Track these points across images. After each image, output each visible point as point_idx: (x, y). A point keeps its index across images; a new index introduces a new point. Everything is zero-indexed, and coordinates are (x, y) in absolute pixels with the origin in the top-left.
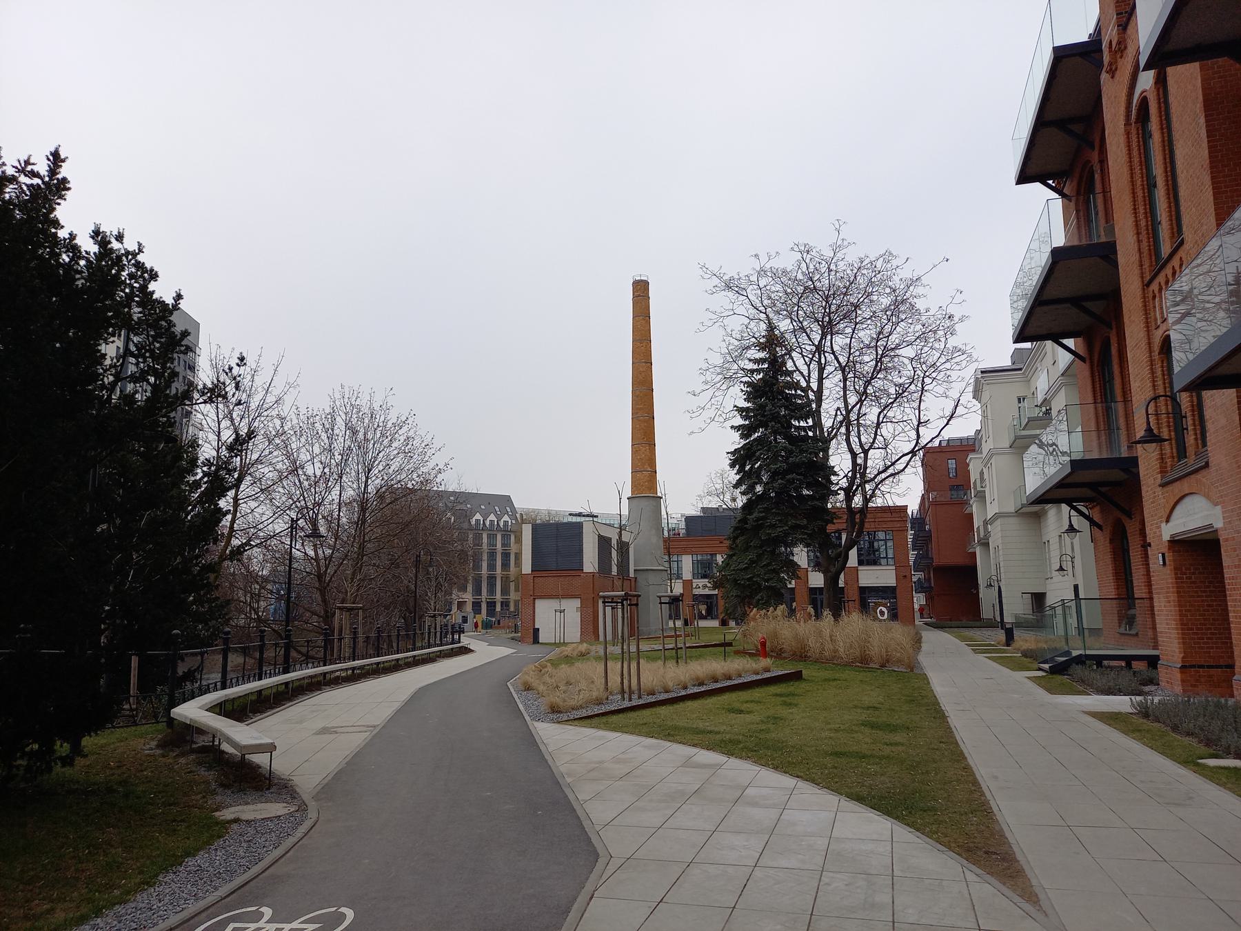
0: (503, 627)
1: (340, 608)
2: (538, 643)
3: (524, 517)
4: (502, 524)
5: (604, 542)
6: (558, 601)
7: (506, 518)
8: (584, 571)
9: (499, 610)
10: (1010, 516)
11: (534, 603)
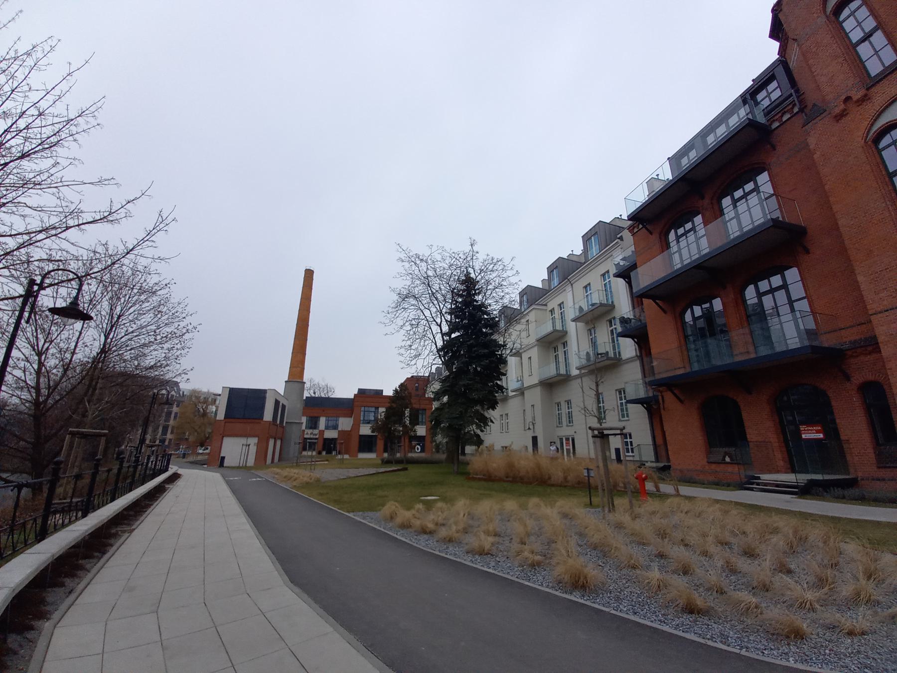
1: (73, 434)
2: (223, 466)
5: (277, 402)
6: (245, 439)
7: (173, 393)
11: (222, 439)
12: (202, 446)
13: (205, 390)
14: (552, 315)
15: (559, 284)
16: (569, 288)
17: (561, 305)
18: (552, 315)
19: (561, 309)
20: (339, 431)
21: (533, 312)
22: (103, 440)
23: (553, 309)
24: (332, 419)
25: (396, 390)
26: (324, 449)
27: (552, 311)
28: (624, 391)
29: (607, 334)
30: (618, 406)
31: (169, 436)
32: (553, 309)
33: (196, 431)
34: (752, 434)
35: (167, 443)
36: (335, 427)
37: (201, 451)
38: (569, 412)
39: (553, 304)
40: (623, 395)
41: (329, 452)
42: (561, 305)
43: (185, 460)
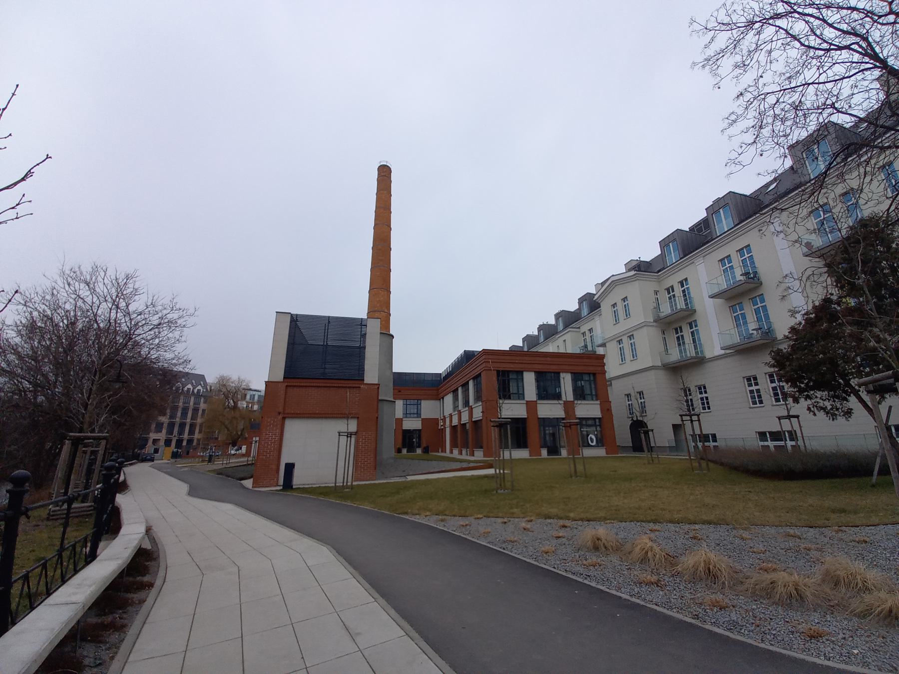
0: (193, 457)
3: (212, 388)
4: (196, 391)
7: (199, 387)
8: (365, 382)
9: (185, 444)
10: (721, 358)
12: (234, 446)
13: (235, 377)
14: (584, 337)
15: (588, 314)
16: (597, 318)
17: (591, 330)
18: (591, 333)
19: (591, 333)
20: (423, 419)
21: (570, 333)
22: (103, 442)
23: (585, 332)
25: (528, 339)
26: (404, 446)
27: (584, 334)
29: (731, 319)
30: (639, 404)
31: (197, 436)
32: (585, 332)
33: (226, 427)
34: (163, 432)
35: (195, 444)
36: (418, 414)
37: (233, 452)
38: (629, 404)
39: (585, 328)
40: (642, 396)
41: (411, 449)
42: (591, 330)
43: (211, 467)
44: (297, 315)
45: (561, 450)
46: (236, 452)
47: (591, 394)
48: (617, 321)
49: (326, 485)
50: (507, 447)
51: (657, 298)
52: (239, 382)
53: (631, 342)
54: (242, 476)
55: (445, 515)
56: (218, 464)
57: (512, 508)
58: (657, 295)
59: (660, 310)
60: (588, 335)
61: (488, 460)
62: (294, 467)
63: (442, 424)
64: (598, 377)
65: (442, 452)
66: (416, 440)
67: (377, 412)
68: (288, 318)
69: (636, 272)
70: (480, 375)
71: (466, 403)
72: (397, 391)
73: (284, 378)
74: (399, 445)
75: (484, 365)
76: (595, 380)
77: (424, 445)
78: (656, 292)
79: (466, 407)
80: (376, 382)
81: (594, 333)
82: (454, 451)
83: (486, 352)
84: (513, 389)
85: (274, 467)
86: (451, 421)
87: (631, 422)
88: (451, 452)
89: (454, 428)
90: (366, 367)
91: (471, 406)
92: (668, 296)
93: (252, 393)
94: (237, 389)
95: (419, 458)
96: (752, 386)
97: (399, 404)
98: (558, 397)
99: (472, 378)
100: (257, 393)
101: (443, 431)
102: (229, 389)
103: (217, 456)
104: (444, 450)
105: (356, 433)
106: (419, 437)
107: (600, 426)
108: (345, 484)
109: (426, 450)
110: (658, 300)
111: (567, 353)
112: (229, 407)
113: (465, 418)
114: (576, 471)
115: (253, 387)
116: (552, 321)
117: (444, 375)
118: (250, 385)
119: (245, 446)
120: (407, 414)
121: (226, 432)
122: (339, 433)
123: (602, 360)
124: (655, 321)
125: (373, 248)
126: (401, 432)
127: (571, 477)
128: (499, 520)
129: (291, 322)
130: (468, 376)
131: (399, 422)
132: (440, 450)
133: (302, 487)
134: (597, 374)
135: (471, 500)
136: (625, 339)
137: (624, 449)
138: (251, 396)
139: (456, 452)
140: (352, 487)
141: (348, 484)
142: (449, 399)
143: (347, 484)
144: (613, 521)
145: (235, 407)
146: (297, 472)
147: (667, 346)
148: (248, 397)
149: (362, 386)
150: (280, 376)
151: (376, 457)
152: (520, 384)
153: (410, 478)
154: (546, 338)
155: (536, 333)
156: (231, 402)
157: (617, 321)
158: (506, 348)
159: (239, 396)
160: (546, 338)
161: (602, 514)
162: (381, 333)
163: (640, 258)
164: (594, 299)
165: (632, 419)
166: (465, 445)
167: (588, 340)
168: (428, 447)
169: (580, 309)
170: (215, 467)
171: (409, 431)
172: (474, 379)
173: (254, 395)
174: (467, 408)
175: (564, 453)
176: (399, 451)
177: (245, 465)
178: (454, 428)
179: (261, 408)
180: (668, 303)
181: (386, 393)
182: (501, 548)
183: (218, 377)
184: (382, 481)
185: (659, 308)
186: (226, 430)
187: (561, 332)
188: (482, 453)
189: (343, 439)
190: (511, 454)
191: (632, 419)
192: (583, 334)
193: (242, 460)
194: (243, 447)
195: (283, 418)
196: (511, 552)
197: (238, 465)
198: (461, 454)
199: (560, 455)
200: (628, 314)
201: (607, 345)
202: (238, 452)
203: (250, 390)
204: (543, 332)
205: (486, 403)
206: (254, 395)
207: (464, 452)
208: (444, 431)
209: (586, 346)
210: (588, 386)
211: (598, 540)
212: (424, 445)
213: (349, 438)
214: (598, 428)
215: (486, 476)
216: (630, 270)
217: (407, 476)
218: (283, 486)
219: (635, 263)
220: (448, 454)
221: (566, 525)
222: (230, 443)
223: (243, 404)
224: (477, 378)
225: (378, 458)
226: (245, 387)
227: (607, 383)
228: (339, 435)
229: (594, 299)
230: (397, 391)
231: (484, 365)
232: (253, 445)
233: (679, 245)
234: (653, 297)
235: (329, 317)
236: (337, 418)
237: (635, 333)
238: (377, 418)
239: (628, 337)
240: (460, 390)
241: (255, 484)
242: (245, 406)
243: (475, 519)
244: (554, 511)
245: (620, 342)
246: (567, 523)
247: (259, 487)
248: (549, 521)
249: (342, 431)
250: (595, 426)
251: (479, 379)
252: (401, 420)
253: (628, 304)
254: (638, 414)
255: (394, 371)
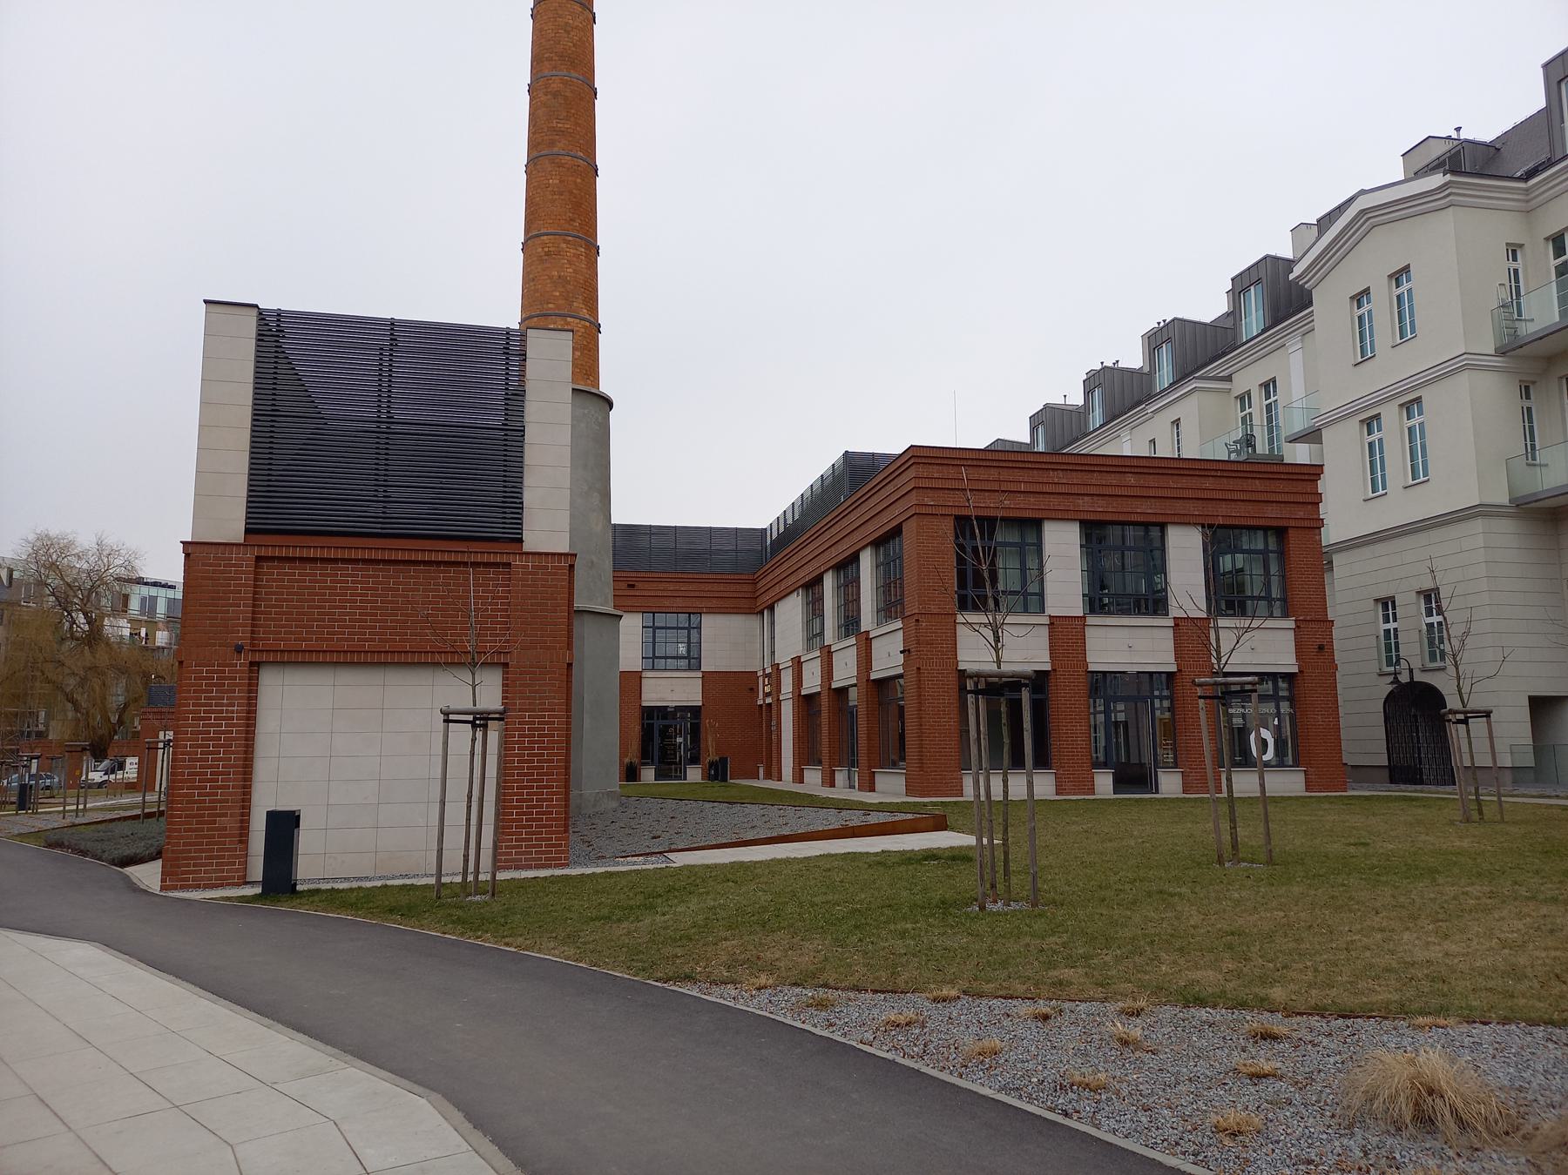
3: (16, 575)
8: (527, 547)
13: (85, 540)
15: (1264, 331)
17: (1269, 386)
18: (1268, 397)
19: (1268, 397)
20: (707, 677)
21: (1194, 397)
23: (1249, 393)
24: (671, 620)
25: (1046, 418)
27: (1244, 399)
28: (1394, 603)
32: (1249, 393)
37: (96, 777)
38: (1387, 632)
39: (1248, 379)
41: (669, 766)
42: (1269, 386)
43: (26, 822)
44: (279, 314)
45: (1160, 774)
46: (106, 778)
47: (1268, 598)
48: (1366, 355)
49: (408, 882)
50: (1018, 762)
51: (1516, 271)
52: (100, 558)
53: (1371, 439)
54: (128, 851)
55: (826, 986)
56: (50, 816)
57: (1052, 965)
58: (1515, 259)
59: (1520, 314)
60: (1258, 402)
61: (925, 805)
62: (298, 825)
63: (767, 689)
64: (1294, 538)
65: (768, 776)
66: (685, 740)
67: (569, 646)
68: (250, 323)
69: (1448, 177)
70: (897, 532)
71: (850, 624)
72: (624, 585)
73: (247, 531)
74: (633, 756)
75: (913, 499)
76: (1282, 554)
77: (710, 754)
78: (1513, 251)
79: (847, 636)
80: (563, 547)
81: (1280, 397)
82: (878, 778)
83: (918, 456)
84: (1008, 577)
85: (230, 822)
86: (798, 681)
87: (1390, 688)
88: (799, 777)
89: (807, 703)
90: (529, 497)
91: (867, 632)
92: (1554, 263)
93: (146, 591)
94: (95, 578)
95: (693, 794)
96: (1432, 616)
97: (632, 627)
98: (1155, 603)
99: (871, 544)
100: (162, 592)
101: (771, 712)
102: (69, 580)
103: (48, 788)
104: (775, 773)
105: (501, 716)
106: (695, 731)
107: (1291, 700)
108: (470, 878)
109: (717, 772)
110: (1517, 281)
111: (1179, 459)
112: (73, 637)
113: (845, 671)
114: (1235, 845)
115: (149, 574)
116: (1133, 358)
117: (775, 535)
118: (137, 563)
119: (136, 760)
120: (654, 657)
121: (70, 715)
122: (446, 714)
123: (1308, 487)
124: (1501, 352)
125: (532, 90)
126: (637, 714)
127: (1220, 861)
128: (1024, 1008)
129: (260, 337)
130: (856, 536)
131: (631, 682)
132: (761, 771)
133: (329, 886)
134: (1290, 531)
135: (903, 935)
136: (1391, 415)
137: (1361, 773)
138: (143, 600)
139: (813, 777)
140: (494, 888)
141: (482, 877)
142: (791, 611)
143: (476, 877)
144: (1441, 1021)
145: (94, 636)
146: (307, 841)
147: (1532, 439)
148: (134, 604)
149: (517, 562)
150: (231, 525)
151: (567, 794)
152: (1032, 563)
153: (680, 859)
154: (1111, 416)
155: (1077, 399)
156: (81, 619)
157: (1366, 355)
158: (981, 444)
159: (104, 602)
160: (1111, 416)
161: (1385, 994)
162: (573, 389)
163: (1458, 129)
164: (1291, 277)
165: (1396, 681)
166: (846, 755)
167: (1259, 418)
168: (723, 761)
169: (1234, 314)
170: (38, 823)
171: (662, 711)
172: (877, 544)
173: (154, 599)
174: (853, 641)
175: (1170, 783)
176: (631, 774)
177: (136, 817)
178: (807, 703)
179: (181, 638)
180: (1554, 284)
181: (594, 591)
182: (1051, 1109)
183: (32, 537)
184: (588, 871)
185: (1519, 305)
186: (69, 705)
187: (1164, 392)
188: (902, 781)
189: (462, 735)
190: (1262, 786)
191: (1396, 681)
192: (1241, 398)
193: (126, 800)
194: (129, 760)
195: (252, 664)
196: (1098, 1127)
197: (114, 815)
198: (832, 785)
199: (1157, 792)
200: (1405, 328)
201: (1326, 434)
202: (112, 777)
203: (140, 581)
204: (1103, 394)
205: (917, 621)
206: (154, 599)
207: (841, 777)
208: (774, 712)
209: (1249, 441)
210: (1258, 570)
211: (1430, 1094)
212: (710, 754)
213: (479, 734)
214: (1285, 707)
215: (930, 855)
216: (1419, 174)
217: (671, 851)
218: (266, 883)
219: (1439, 150)
220: (787, 783)
221: (1276, 1030)
222: (84, 749)
223: (119, 628)
224: (885, 541)
225: (574, 793)
226: (122, 572)
227: (1322, 561)
228: (447, 721)
229: (1291, 277)
230: (624, 585)
231: (913, 499)
232: (160, 752)
233: (1199, 350)
234: (1504, 265)
235: (393, 323)
236: (436, 664)
237: (1425, 394)
238: (570, 665)
239: (1362, 421)
240: (829, 581)
241: (171, 878)
242: (126, 632)
243: (935, 1000)
244: (1208, 978)
245: (1371, 423)
246: (1277, 1024)
247: (183, 888)
248: (1203, 1014)
249: (453, 707)
250: (1275, 698)
251: (893, 546)
252: (638, 676)
253: (1370, 312)
254: (1416, 664)
255: (616, 519)
